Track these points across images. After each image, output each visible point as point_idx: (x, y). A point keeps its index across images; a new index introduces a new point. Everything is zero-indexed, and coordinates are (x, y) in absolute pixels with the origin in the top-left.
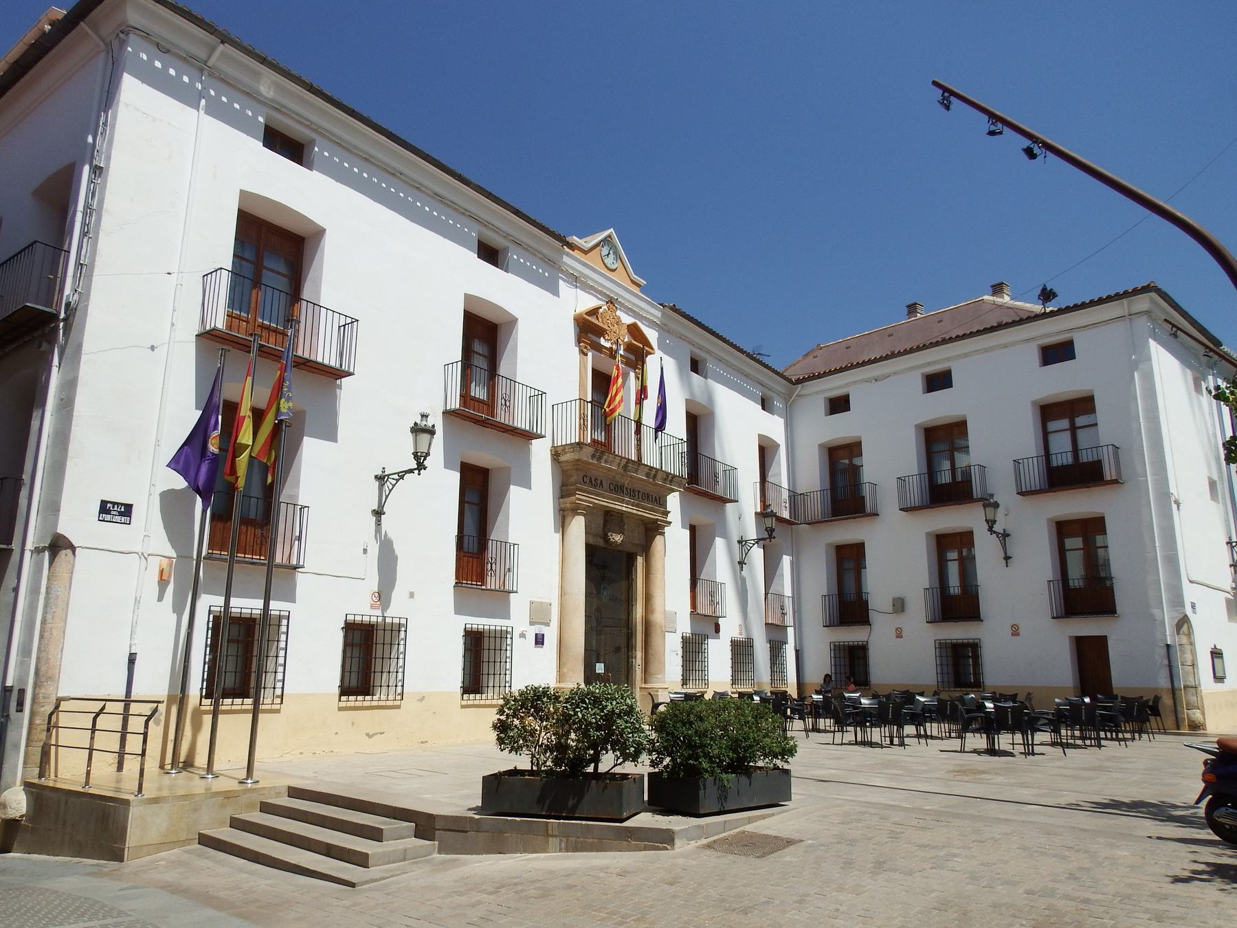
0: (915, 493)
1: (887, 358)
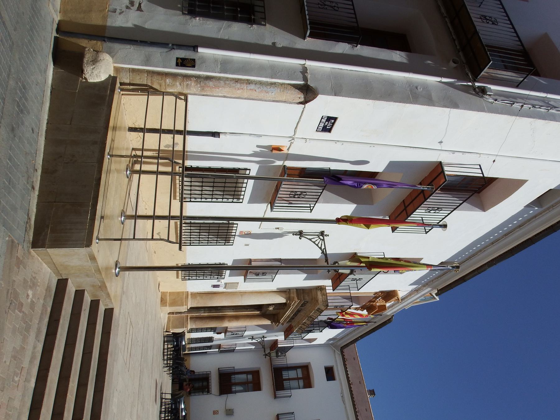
1: (348, 381)
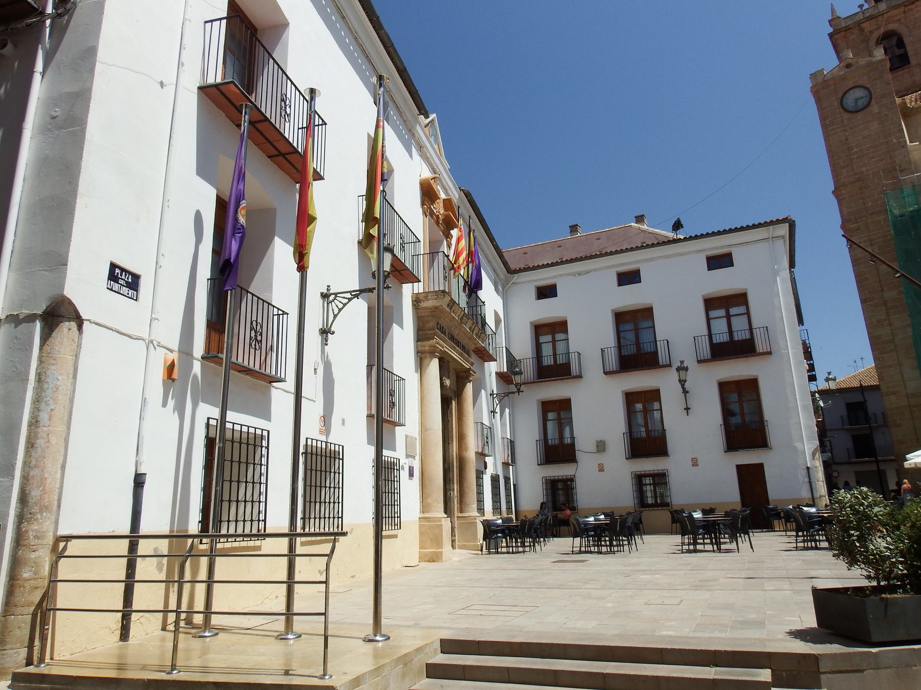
0: (613, 361)
